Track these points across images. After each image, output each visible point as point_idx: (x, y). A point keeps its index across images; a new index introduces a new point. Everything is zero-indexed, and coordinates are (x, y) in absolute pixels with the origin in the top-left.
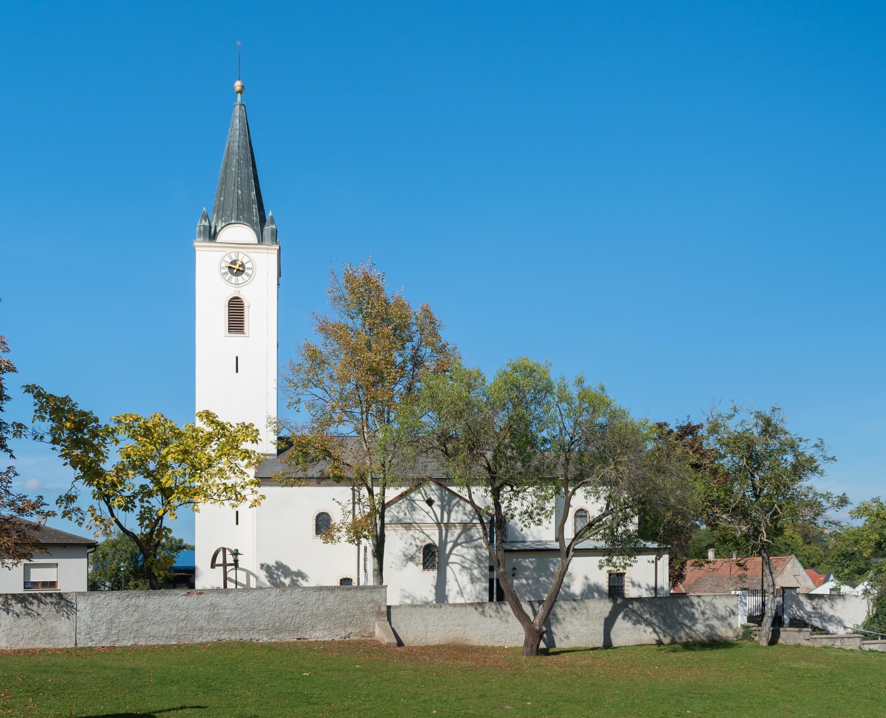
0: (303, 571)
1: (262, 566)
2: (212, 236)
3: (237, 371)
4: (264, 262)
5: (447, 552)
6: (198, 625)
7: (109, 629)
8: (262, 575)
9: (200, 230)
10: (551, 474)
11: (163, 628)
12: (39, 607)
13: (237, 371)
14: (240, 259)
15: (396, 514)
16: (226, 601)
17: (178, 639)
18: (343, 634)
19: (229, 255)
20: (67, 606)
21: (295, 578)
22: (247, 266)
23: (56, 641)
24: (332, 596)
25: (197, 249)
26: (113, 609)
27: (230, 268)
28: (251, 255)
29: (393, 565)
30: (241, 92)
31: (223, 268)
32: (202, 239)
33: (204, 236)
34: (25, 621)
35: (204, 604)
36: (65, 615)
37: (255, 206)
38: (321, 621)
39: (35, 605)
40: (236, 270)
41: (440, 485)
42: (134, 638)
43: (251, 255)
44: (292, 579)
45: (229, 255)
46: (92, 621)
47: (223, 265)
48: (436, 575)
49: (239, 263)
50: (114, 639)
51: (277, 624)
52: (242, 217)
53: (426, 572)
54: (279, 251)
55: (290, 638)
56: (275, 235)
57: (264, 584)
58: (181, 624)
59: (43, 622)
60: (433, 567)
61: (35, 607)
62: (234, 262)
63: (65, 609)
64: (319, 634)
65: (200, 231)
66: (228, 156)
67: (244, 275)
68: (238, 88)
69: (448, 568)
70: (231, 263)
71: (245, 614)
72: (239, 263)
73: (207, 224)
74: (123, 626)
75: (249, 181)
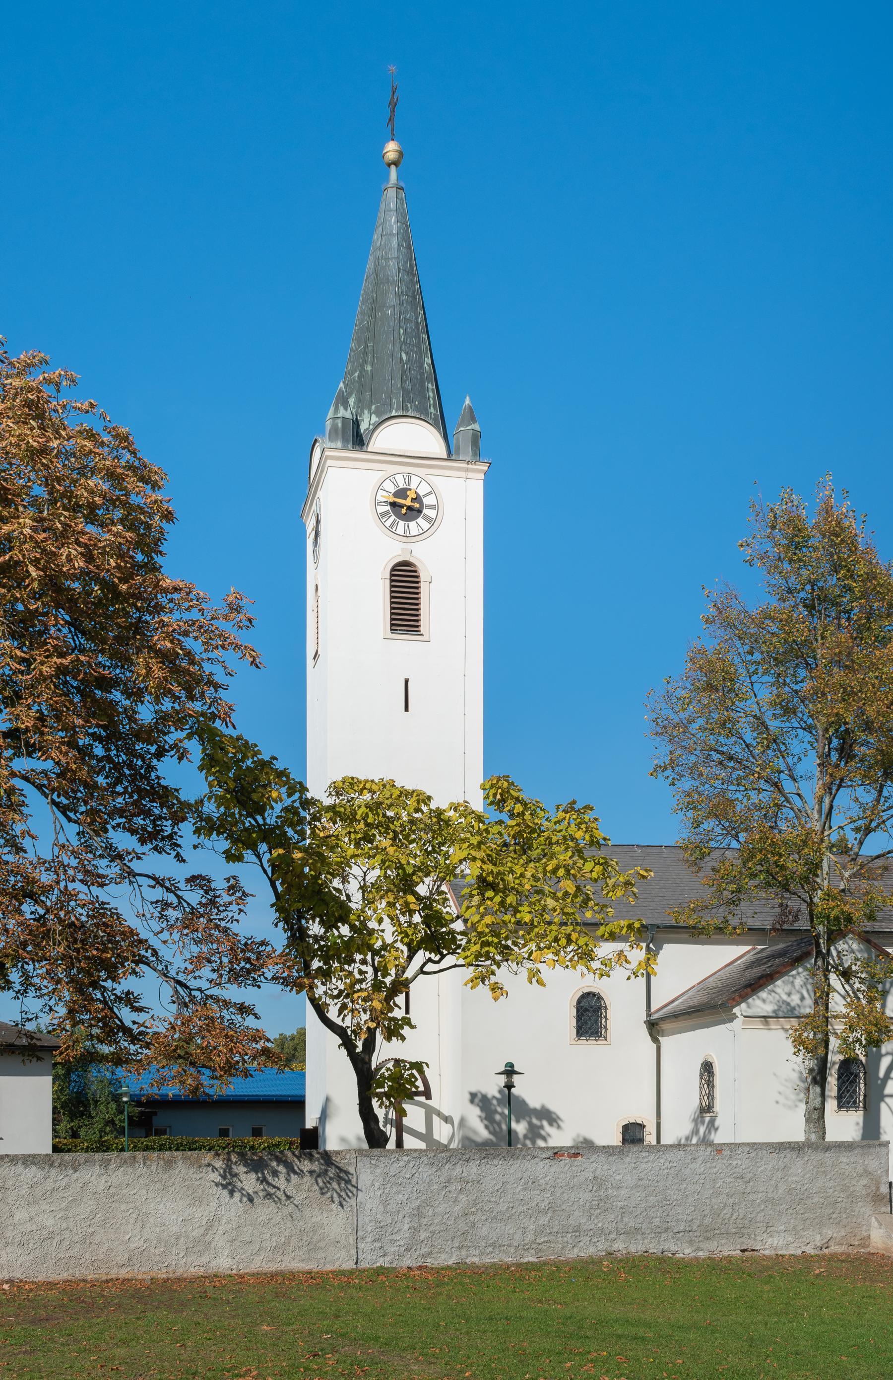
0: (552, 1107)
1: (473, 1096)
2: (357, 439)
4: (460, 496)
5: (882, 1074)
6: (571, 1221)
7: (415, 1230)
8: (474, 1116)
11: (510, 1228)
12: (288, 1180)
13: (407, 709)
14: (413, 486)
15: (785, 997)
16: (625, 1171)
17: (538, 1251)
18: (818, 1240)
19: (392, 478)
20: (339, 1179)
21: (535, 1121)
22: (426, 501)
23: (321, 1255)
24: (800, 1162)
26: (422, 1188)
27: (393, 505)
28: (434, 480)
29: (781, 1099)
30: (396, 163)
32: (339, 444)
33: (344, 440)
34: (265, 1211)
35: (582, 1178)
36: (336, 1199)
38: (780, 1213)
39: (282, 1177)
40: (405, 507)
41: (868, 941)
42: (460, 1248)
43: (434, 480)
44: (530, 1124)
45: (392, 478)
46: (385, 1212)
47: (382, 496)
48: (861, 1120)
50: (424, 1250)
51: (708, 1220)
53: (843, 1113)
55: (729, 1249)
57: (475, 1132)
58: (544, 1220)
59: (297, 1215)
60: (855, 1106)
61: (281, 1182)
62: (402, 493)
63: (335, 1185)
64: (778, 1242)
65: (334, 429)
67: (420, 520)
69: (883, 1106)
70: (396, 495)
71: (652, 1199)
74: (441, 1223)
75: (418, 337)
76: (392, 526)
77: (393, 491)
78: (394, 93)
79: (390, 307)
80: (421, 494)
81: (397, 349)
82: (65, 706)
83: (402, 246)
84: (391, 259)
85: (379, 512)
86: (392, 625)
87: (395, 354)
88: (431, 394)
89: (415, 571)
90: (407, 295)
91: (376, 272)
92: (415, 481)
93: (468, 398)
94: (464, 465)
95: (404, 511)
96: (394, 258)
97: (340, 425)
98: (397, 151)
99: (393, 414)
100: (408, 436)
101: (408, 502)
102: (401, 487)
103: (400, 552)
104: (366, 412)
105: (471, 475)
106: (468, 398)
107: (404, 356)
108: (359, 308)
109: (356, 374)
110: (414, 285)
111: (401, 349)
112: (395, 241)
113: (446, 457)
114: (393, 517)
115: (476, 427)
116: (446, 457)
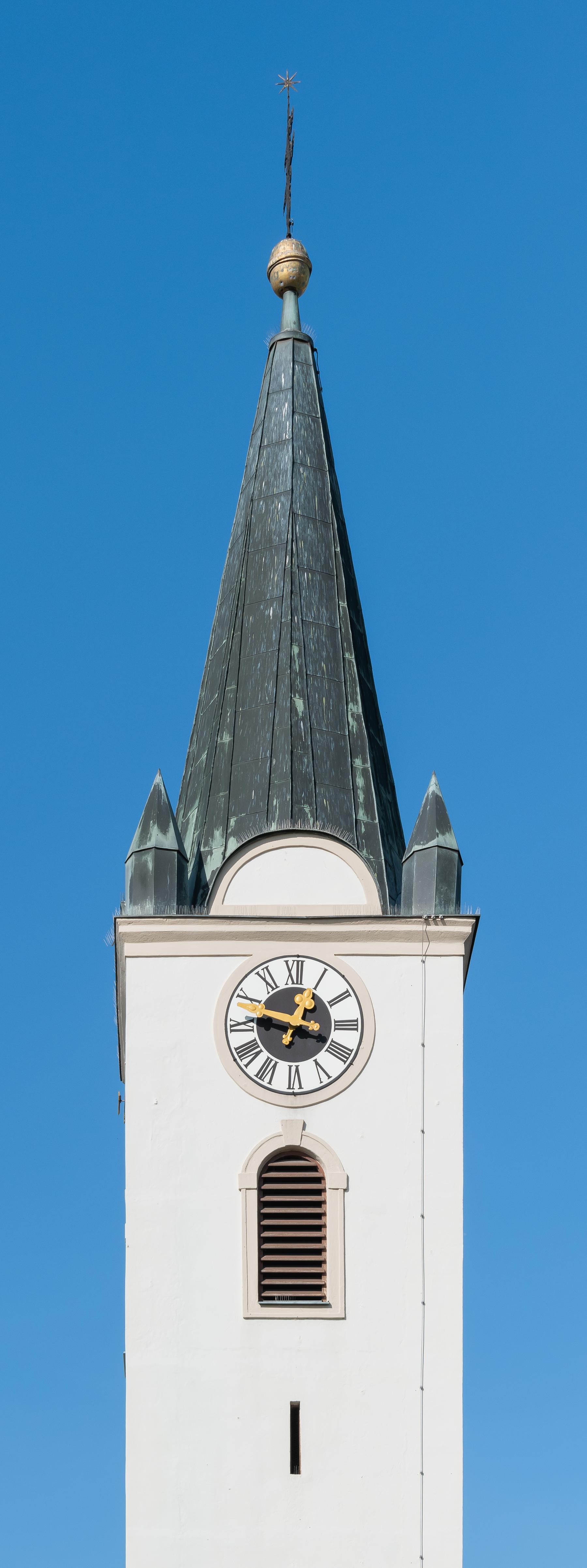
2: (190, 891)
3: (295, 1466)
4: (411, 996)
9: (140, 869)
10: (281, 443)
13: (295, 1466)
14: (308, 983)
19: (262, 969)
22: (337, 1013)
25: (128, 948)
27: (265, 1023)
28: (356, 966)
30: (295, 286)
31: (235, 1027)
32: (149, 907)
33: (160, 897)
37: (362, 764)
40: (291, 1031)
43: (356, 966)
45: (262, 969)
47: (238, 1013)
49: (304, 1002)
52: (309, 811)
54: (470, 943)
56: (451, 871)
62: (283, 999)
66: (246, 559)
67: (323, 1057)
68: (285, 272)
70: (271, 1003)
72: (304, 1002)
73: (169, 841)
75: (335, 659)
76: (261, 1074)
77: (264, 997)
78: (289, 134)
79: (272, 599)
80: (326, 997)
81: (284, 688)
83: (303, 464)
84: (278, 495)
85: (234, 1045)
86: (262, 1288)
87: (280, 701)
88: (360, 782)
89: (315, 1169)
90: (310, 570)
91: (248, 528)
92: (312, 971)
93: (433, 780)
94: (417, 927)
95: (287, 1039)
96: (284, 493)
97: (150, 866)
98: (294, 259)
99: (274, 828)
100: (308, 874)
101: (296, 1019)
102: (282, 986)
103: (279, 1130)
104: (218, 833)
105: (435, 947)
106: (433, 780)
107: (300, 704)
108: (216, 614)
109: (204, 756)
110: (328, 547)
111: (292, 689)
112: (286, 458)
113: (379, 913)
114: (265, 1055)
115: (449, 840)
116: (379, 913)
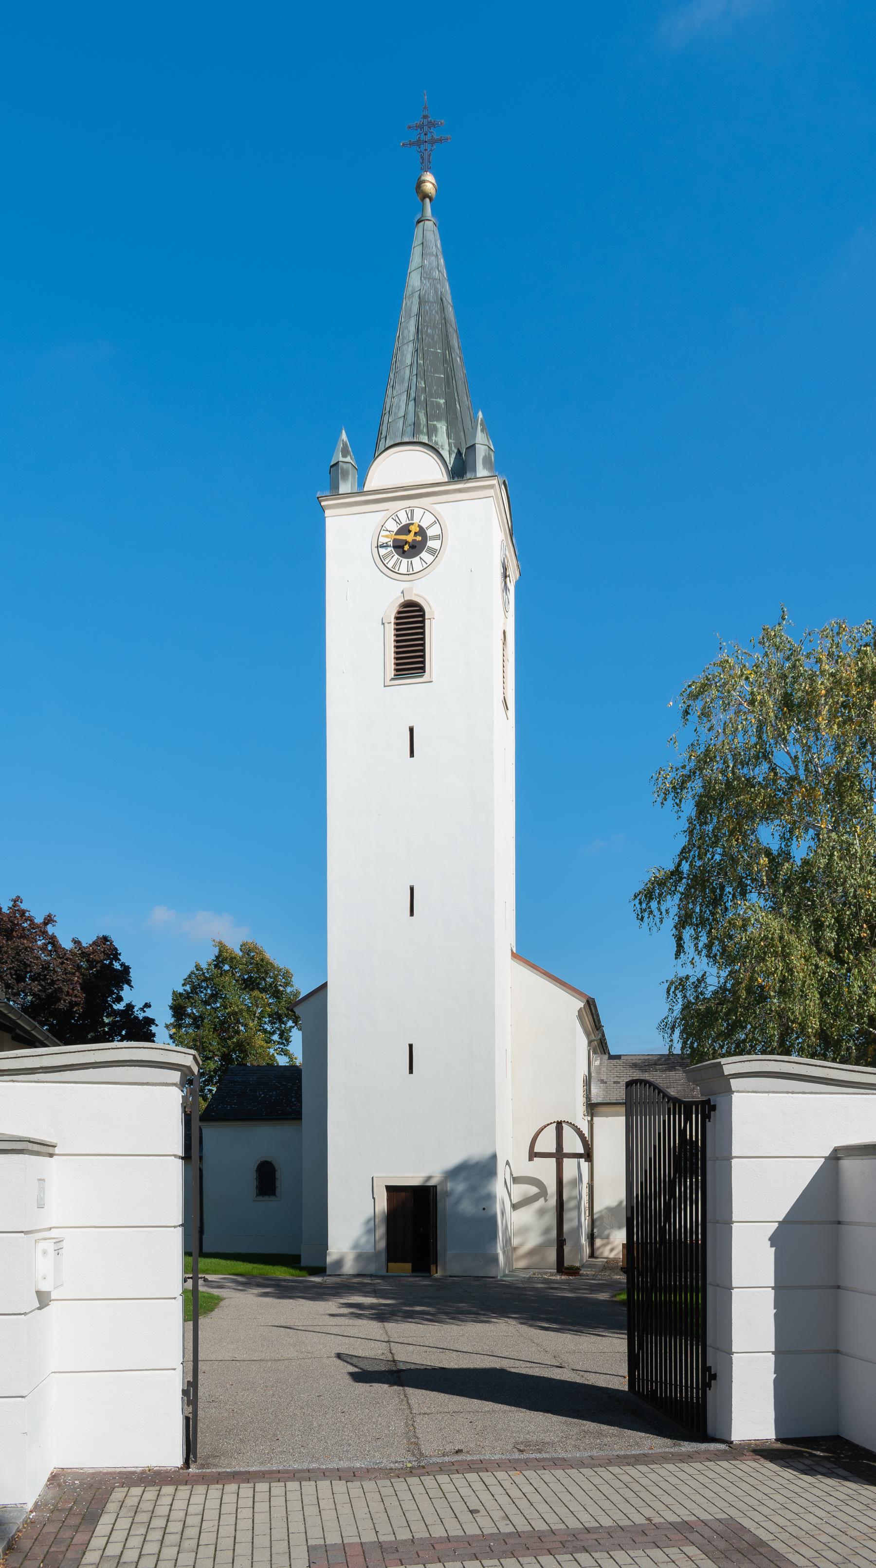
3: (412, 754)
13: (412, 754)
14: (416, 520)
22: (430, 533)
28: (440, 509)
43: (440, 509)
49: (414, 529)
62: (405, 530)
67: (424, 555)
72: (414, 529)
80: (424, 527)
82: (841, 846)
92: (418, 513)
102: (404, 523)
114: (396, 556)
